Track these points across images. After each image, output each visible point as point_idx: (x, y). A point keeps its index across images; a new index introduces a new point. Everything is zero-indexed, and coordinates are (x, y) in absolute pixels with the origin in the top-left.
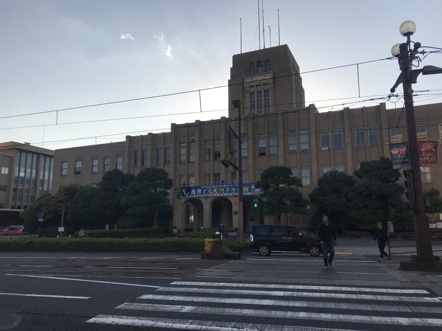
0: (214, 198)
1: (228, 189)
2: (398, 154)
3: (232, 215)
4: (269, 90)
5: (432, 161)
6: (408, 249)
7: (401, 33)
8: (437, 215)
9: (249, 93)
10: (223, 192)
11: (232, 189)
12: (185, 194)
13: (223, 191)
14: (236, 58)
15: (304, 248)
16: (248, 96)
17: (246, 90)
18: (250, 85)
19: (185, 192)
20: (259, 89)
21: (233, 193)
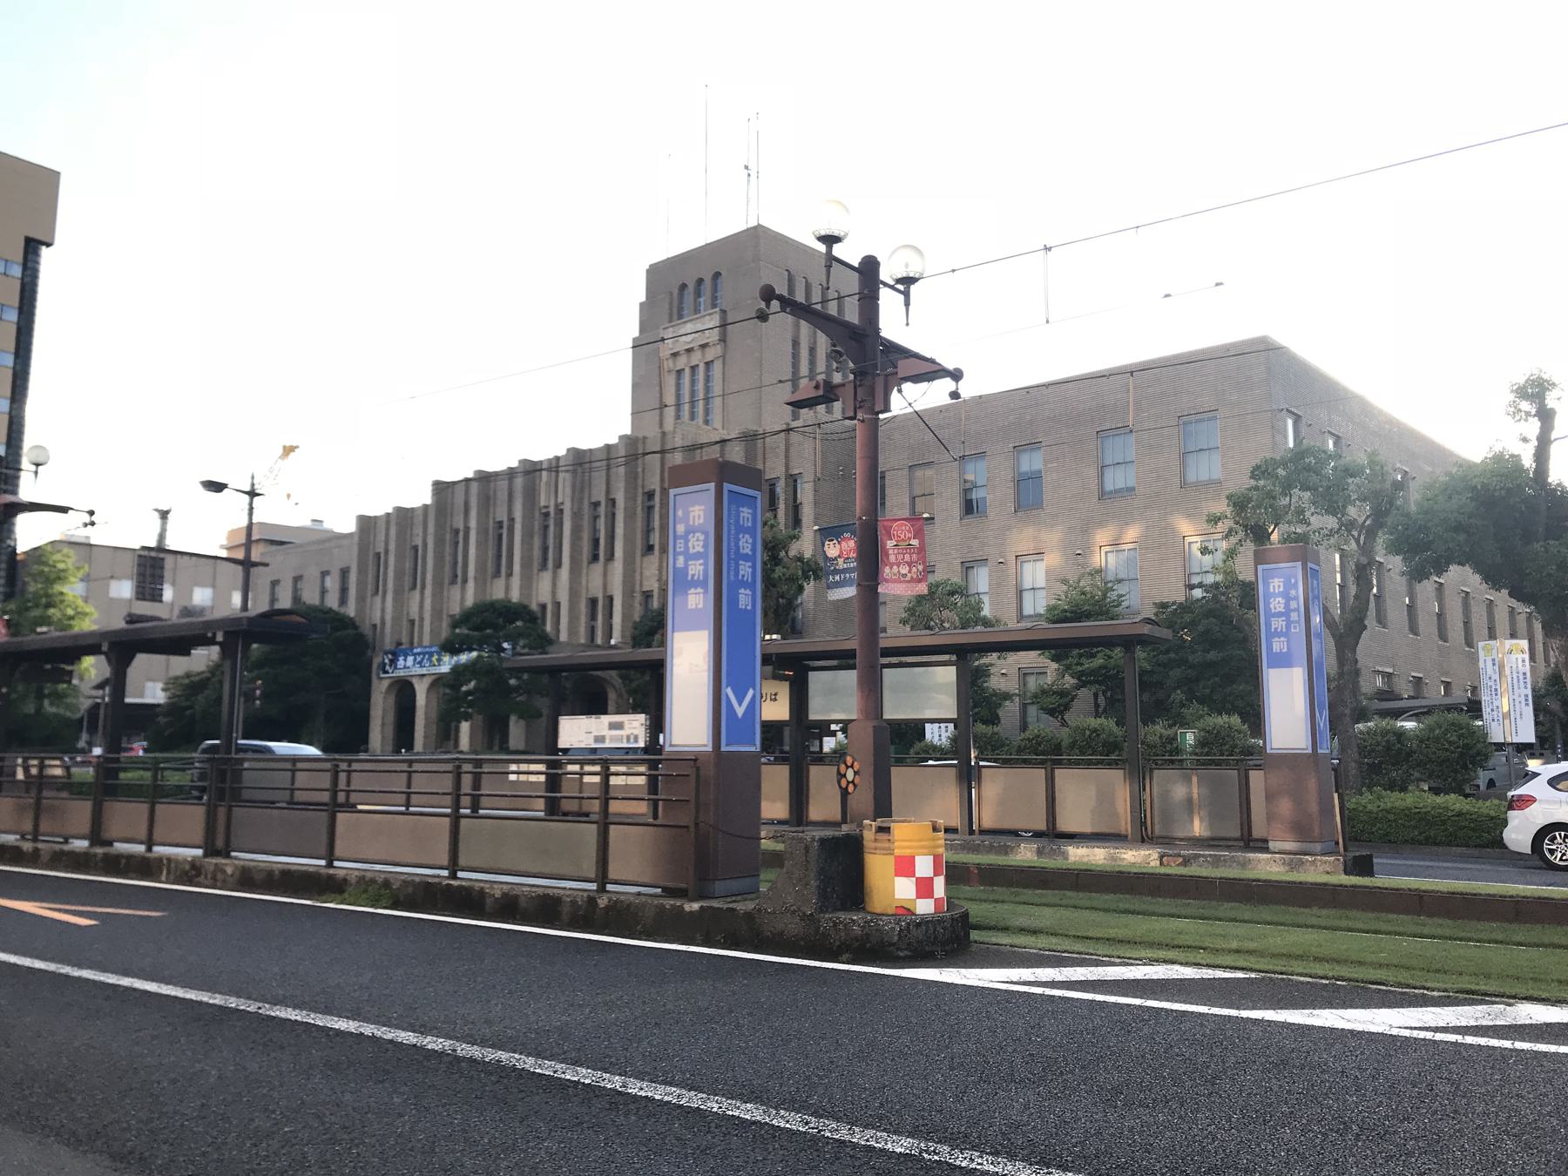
0: (433, 677)
2: (839, 556)
5: (915, 577)
18: (672, 352)
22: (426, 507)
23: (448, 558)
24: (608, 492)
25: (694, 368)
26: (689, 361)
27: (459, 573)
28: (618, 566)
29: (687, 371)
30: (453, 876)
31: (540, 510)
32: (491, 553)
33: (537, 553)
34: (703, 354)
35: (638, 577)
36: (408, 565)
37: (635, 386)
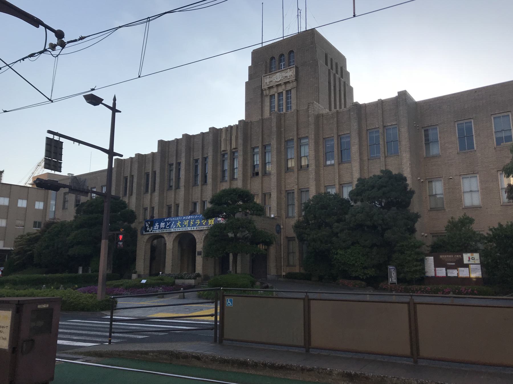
0: (178, 233)
1: (192, 222)
3: (195, 256)
4: (292, 90)
6: (201, 306)
8: (460, 256)
9: (277, 93)
10: (187, 226)
11: (197, 221)
12: (148, 229)
13: (187, 225)
14: (256, 54)
16: (267, 100)
17: (264, 92)
18: (268, 86)
19: (149, 226)
20: (280, 90)
21: (197, 226)
22: (153, 154)
25: (280, 94)
28: (182, 192)
29: (276, 95)
32: (192, 175)
33: (219, 173)
34: (285, 87)
36: (143, 181)
37: (247, 104)
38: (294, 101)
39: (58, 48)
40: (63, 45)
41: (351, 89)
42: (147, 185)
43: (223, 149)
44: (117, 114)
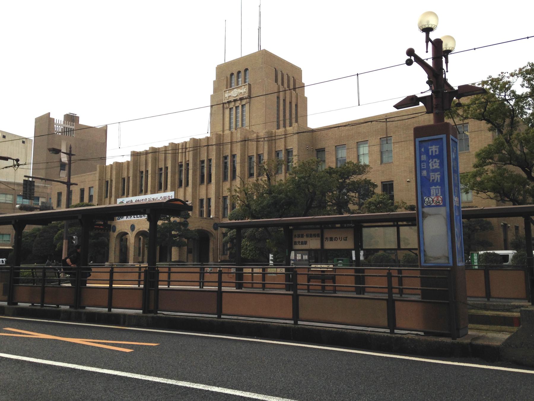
3: (292, 245)
4: (246, 105)
7: (419, 28)
9: (229, 109)
15: (353, 253)
18: (228, 100)
23: (138, 183)
24: (208, 156)
26: (229, 106)
27: (143, 188)
28: (190, 189)
30: (296, 323)
31: (178, 163)
35: (221, 191)
36: (121, 185)
38: (247, 114)
39: (17, 166)
40: (18, 165)
41: (305, 100)
42: (124, 190)
43: (179, 161)
44: (72, 157)
